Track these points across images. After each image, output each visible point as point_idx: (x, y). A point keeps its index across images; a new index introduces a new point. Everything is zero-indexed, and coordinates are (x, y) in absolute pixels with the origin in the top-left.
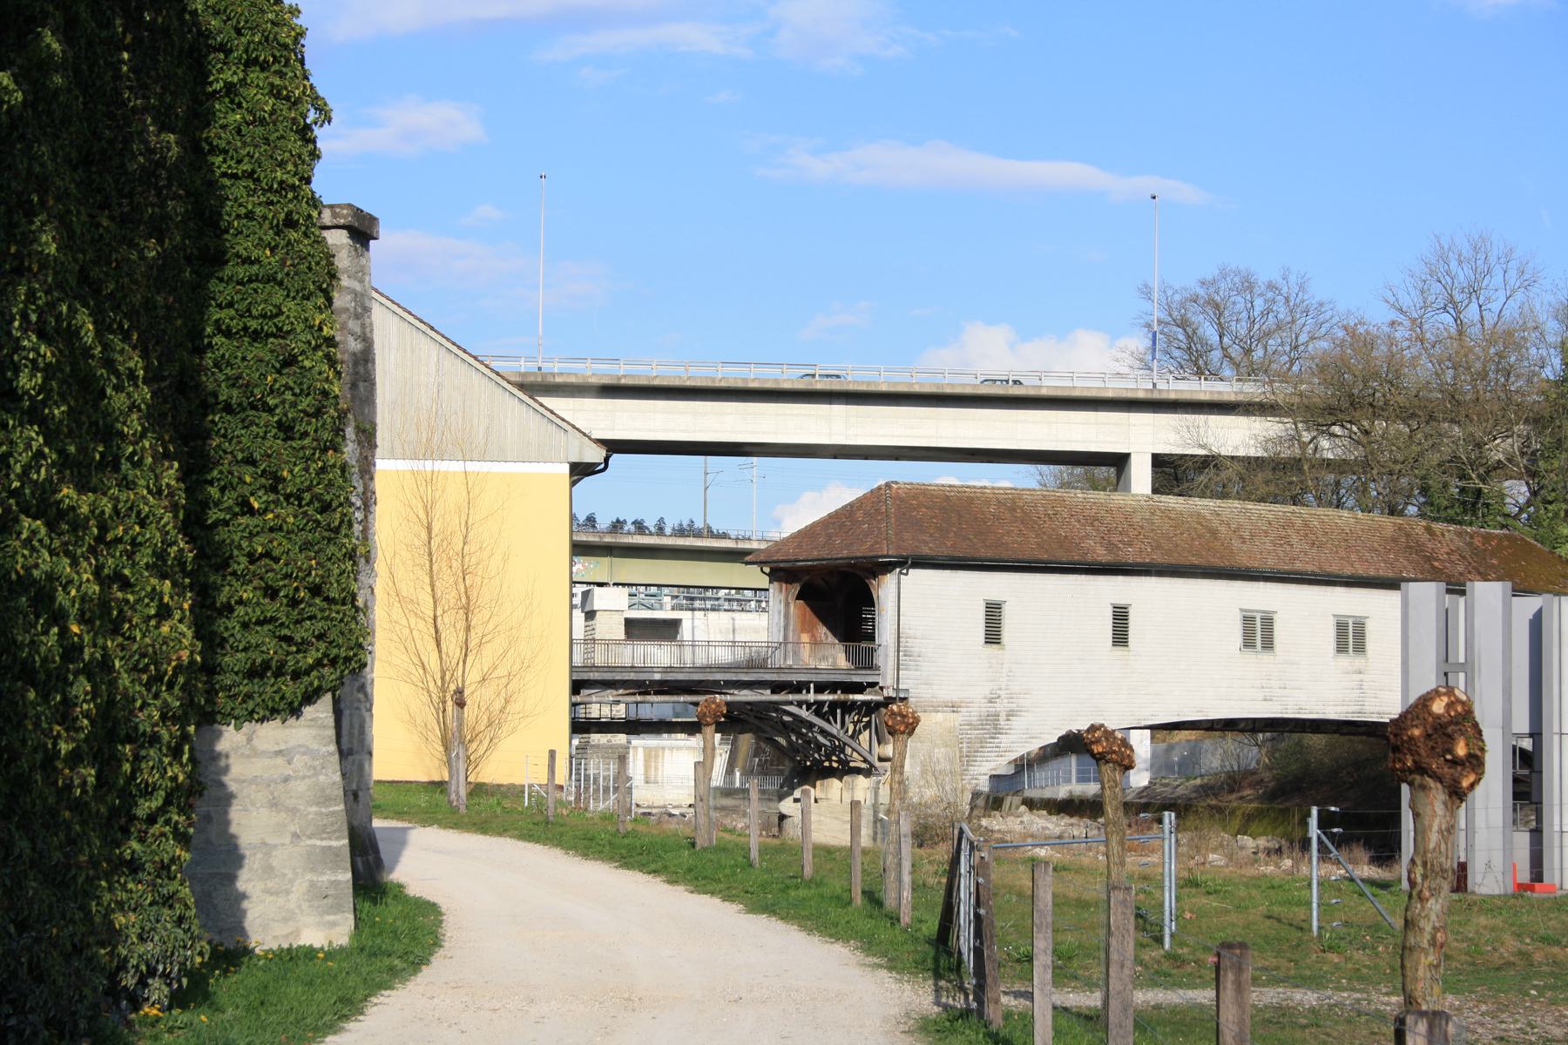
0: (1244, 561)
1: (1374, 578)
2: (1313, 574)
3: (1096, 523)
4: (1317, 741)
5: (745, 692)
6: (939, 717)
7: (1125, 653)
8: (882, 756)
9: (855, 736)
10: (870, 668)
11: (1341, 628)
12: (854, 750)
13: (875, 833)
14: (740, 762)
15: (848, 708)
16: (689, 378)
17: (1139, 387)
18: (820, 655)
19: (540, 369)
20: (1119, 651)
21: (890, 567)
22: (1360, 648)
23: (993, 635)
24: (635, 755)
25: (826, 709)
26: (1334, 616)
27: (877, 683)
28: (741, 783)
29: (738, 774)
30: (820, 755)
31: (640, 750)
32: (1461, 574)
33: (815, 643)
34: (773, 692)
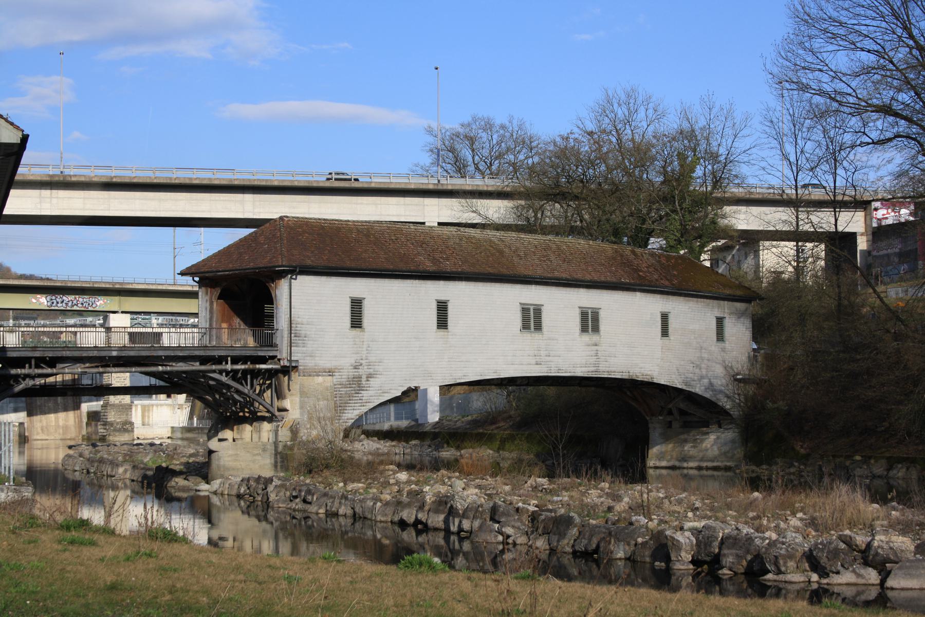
0: (522, 271)
1: (604, 282)
2: (567, 279)
3: (424, 245)
4: (551, 391)
5: (181, 364)
6: (320, 379)
7: (446, 333)
8: (280, 407)
9: (261, 394)
10: (272, 346)
11: (584, 315)
12: (260, 404)
13: (276, 462)
14: (197, 412)
15: (256, 374)
16: (156, 178)
17: (430, 183)
18: (234, 338)
19: (62, 172)
20: (442, 332)
21: (284, 274)
22: (596, 329)
23: (356, 322)
24: (136, 410)
25: (240, 375)
26: (580, 307)
27: (276, 357)
28: (197, 424)
29: (195, 419)
30: (236, 408)
31: (139, 407)
32: (657, 280)
33: (231, 329)
34: (201, 364)
